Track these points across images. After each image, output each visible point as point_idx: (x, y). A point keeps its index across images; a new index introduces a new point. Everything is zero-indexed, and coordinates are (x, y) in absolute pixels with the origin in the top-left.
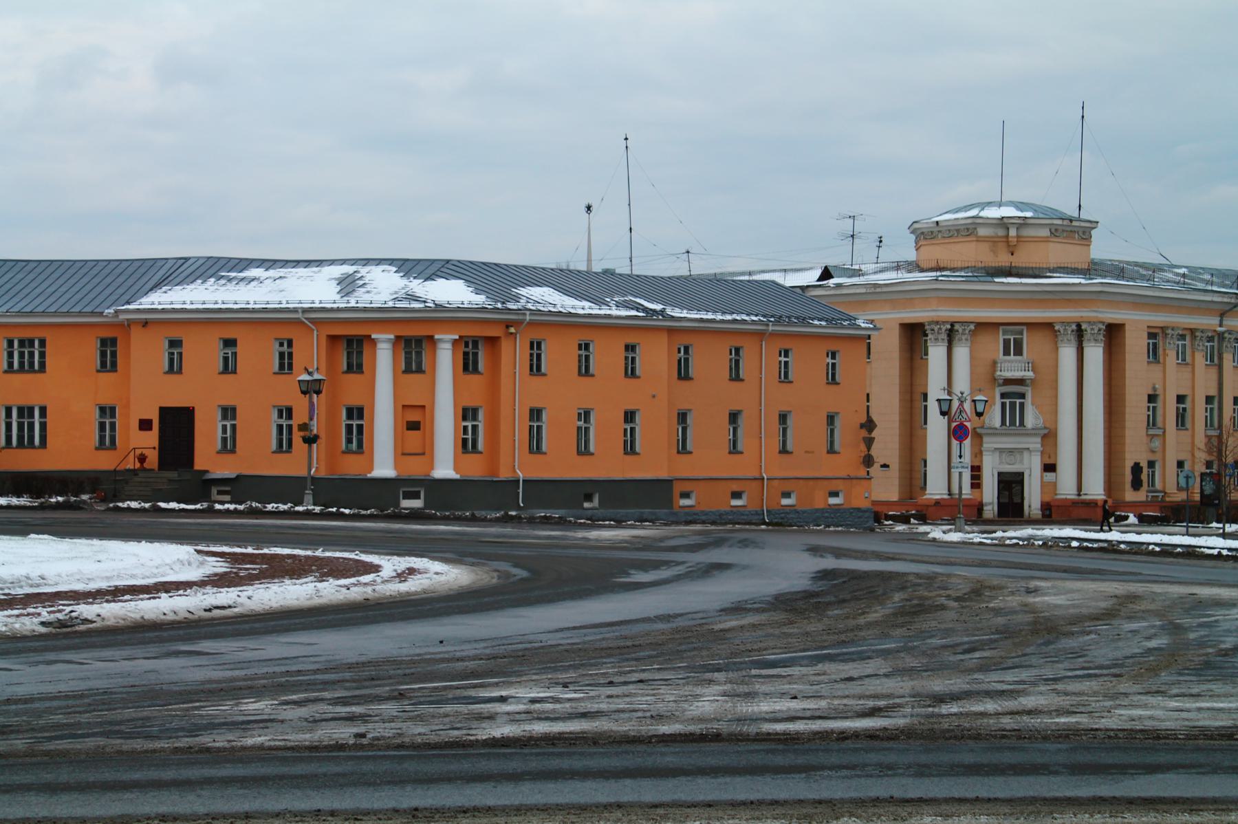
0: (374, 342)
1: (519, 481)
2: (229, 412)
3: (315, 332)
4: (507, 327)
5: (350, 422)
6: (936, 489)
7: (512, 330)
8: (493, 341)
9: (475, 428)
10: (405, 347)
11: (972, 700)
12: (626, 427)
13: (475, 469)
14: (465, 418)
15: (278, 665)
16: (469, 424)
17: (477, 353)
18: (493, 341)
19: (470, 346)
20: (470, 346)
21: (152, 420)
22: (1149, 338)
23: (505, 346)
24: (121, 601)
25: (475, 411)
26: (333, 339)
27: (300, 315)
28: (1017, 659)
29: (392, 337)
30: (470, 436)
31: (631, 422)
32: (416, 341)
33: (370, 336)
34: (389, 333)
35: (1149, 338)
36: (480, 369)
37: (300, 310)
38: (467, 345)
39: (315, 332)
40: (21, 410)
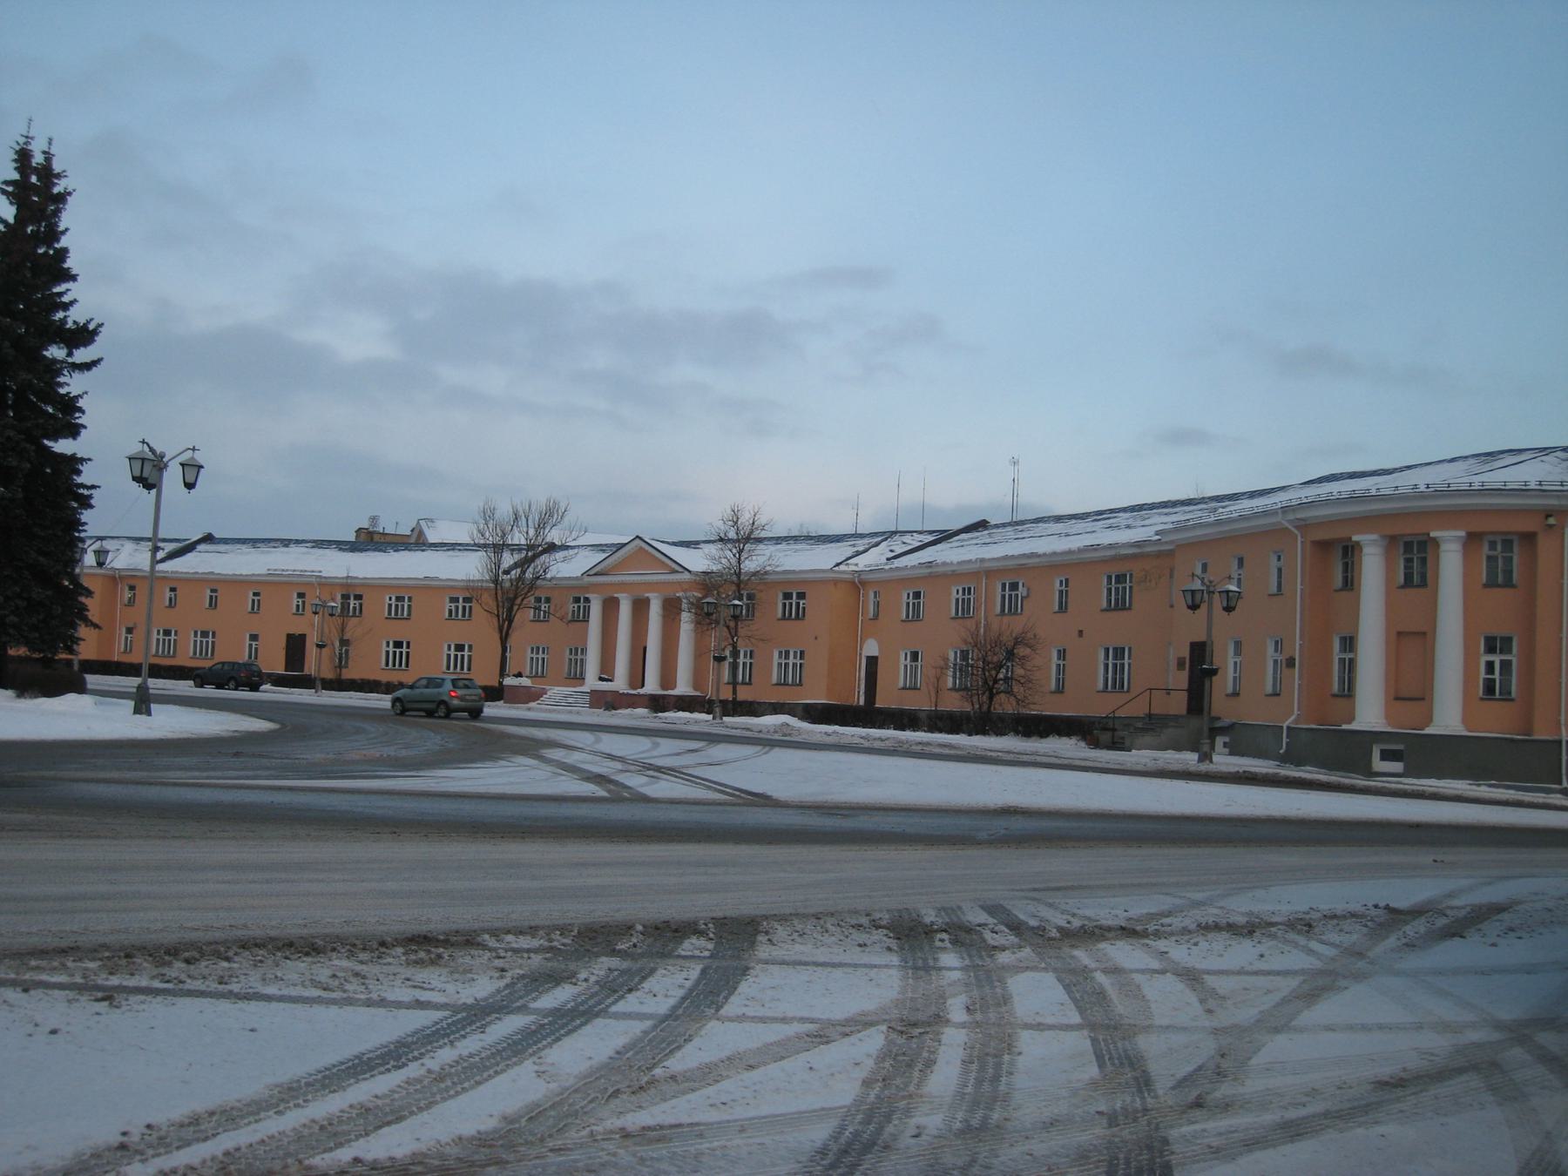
0: (1435, 543)
1: (1560, 742)
2: (254, 637)
3: (1299, 538)
4: (1548, 516)
5: (1490, 658)
6: (683, 688)
7: (1552, 521)
8: (1529, 538)
9: (1506, 665)
10: (1405, 552)
11: (651, 922)
12: (1236, 660)
13: (1496, 724)
14: (1491, 649)
15: (267, 882)
16: (1496, 659)
17: (1511, 559)
18: (1529, 538)
19: (1499, 548)
20: (1499, 548)
21: (289, 636)
22: (451, 602)
23: (1544, 544)
24: (812, 1021)
25: (1508, 641)
26: (1323, 546)
27: (1279, 518)
28: (279, 761)
29: (1462, 533)
30: (1497, 675)
31: (1351, 651)
32: (1419, 543)
33: (1351, 538)
34: (1455, 528)
35: (451, 602)
36: (1514, 582)
37: (1280, 511)
38: (1493, 545)
39: (1299, 538)
40: (1115, 649)
